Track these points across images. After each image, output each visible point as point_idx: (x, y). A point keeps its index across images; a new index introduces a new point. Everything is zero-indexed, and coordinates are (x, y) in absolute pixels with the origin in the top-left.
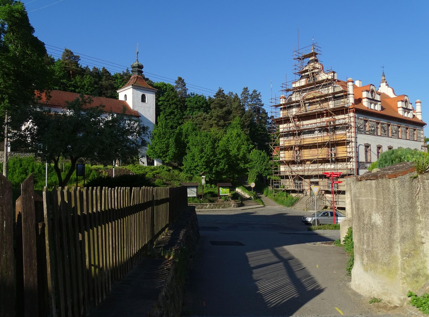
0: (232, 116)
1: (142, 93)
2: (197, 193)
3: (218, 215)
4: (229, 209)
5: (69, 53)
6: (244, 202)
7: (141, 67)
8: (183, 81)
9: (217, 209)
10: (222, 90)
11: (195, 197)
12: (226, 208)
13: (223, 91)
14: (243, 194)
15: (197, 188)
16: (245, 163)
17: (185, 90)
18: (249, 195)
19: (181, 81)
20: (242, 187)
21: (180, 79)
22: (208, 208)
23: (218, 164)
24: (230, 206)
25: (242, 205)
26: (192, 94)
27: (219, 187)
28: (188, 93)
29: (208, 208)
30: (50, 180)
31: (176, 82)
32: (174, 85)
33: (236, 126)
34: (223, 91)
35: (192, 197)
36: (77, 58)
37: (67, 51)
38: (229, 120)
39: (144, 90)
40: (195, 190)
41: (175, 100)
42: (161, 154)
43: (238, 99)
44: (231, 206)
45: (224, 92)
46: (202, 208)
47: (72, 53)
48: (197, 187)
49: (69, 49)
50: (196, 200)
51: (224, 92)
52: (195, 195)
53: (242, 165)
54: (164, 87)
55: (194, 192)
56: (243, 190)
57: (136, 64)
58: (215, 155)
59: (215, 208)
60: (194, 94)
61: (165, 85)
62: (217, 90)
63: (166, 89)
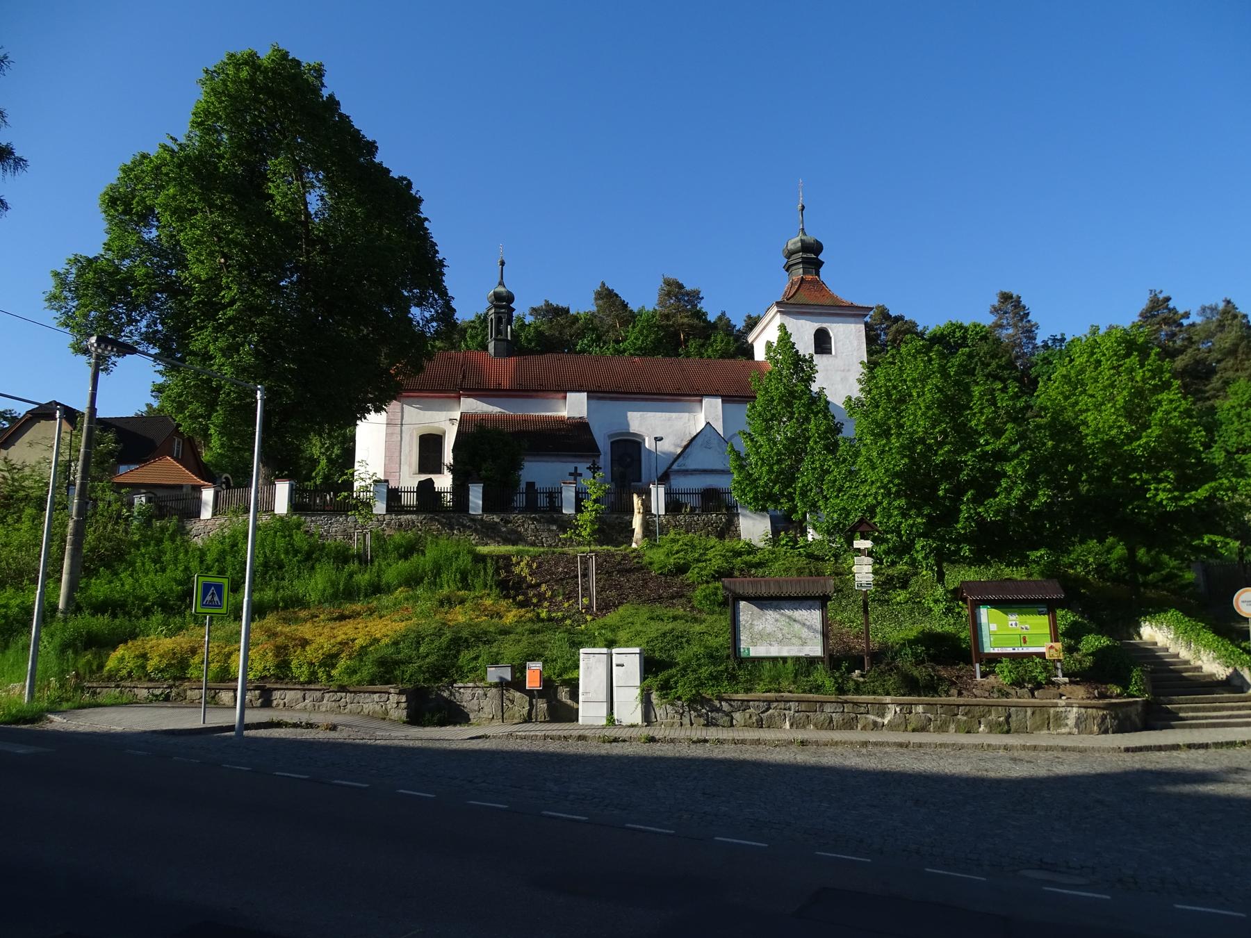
0: (1215, 382)
1: (817, 326)
2: (825, 635)
3: (757, 765)
4: (1043, 738)
5: (674, 290)
6: (1179, 704)
7: (816, 248)
8: (1017, 304)
9: (952, 737)
10: (1161, 297)
11: (812, 661)
12: (1022, 730)
13: (1168, 299)
14: (1184, 654)
15: (823, 607)
16: (1186, 483)
17: (1030, 333)
18: (1227, 660)
19: (1010, 304)
20: (1172, 614)
21: (1006, 297)
22: (892, 727)
23: (985, 486)
24: (1052, 721)
25: (1155, 716)
26: (1055, 340)
27: (976, 605)
28: (1041, 337)
29: (892, 727)
30: (256, 596)
31: (995, 310)
32: (988, 320)
33: (1239, 415)
34: (1168, 299)
35: (797, 659)
36: (695, 296)
37: (668, 283)
38: (1208, 399)
39: (821, 314)
40: (814, 617)
41: (994, 364)
42: (776, 489)
43: (1235, 317)
44: (1059, 720)
45: (1171, 304)
46: (849, 725)
47: (681, 286)
48: (821, 601)
49: (672, 276)
50: (821, 675)
51: (1171, 304)
52: (816, 650)
53: (1162, 495)
54: (958, 334)
55: (805, 633)
56: (1185, 635)
57: (794, 242)
58: (966, 438)
59: (942, 728)
60: (1063, 340)
61: (961, 327)
62: (1143, 303)
63: (964, 338)
